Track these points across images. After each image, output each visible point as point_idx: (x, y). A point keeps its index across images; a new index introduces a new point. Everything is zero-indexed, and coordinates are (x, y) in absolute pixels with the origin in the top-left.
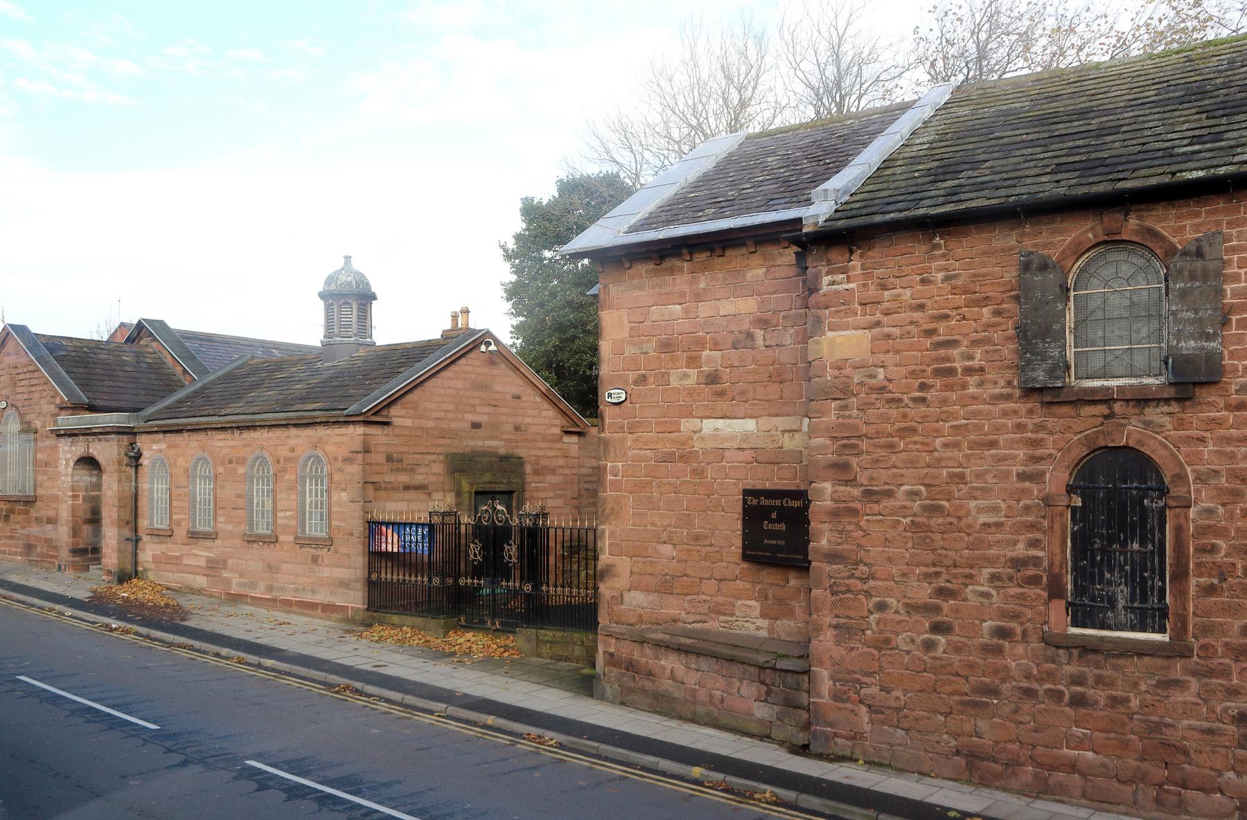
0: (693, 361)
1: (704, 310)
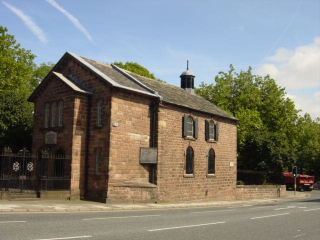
0: (130, 120)
1: (133, 108)
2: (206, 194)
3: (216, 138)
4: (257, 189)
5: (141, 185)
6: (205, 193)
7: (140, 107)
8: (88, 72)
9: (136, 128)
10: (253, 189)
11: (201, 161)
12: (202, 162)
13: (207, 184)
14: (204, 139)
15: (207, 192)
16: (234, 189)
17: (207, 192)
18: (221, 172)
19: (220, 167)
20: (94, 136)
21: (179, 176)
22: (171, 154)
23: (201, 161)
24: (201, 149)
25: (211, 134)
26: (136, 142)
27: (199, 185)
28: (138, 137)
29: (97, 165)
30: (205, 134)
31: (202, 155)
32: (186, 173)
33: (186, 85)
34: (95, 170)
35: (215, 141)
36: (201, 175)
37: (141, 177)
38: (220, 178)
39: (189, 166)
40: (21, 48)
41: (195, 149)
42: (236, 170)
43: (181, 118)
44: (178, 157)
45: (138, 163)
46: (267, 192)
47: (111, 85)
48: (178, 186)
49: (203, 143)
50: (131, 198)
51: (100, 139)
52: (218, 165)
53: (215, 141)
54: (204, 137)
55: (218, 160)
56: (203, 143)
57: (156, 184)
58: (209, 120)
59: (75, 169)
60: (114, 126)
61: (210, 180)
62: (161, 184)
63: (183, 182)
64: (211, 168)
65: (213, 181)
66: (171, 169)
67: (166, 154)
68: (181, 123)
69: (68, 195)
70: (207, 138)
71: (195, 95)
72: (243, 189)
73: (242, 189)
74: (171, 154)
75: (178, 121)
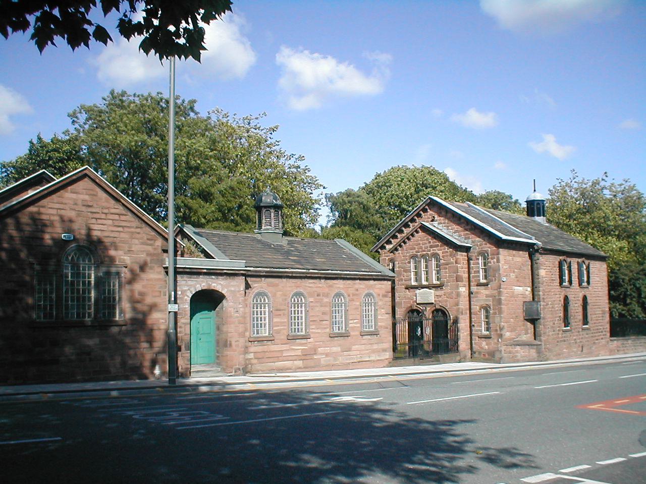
2: (582, 351)
3: (588, 282)
4: (630, 342)
5: (529, 343)
6: (580, 349)
7: (520, 256)
8: (462, 221)
9: (519, 282)
10: (625, 342)
11: (576, 308)
12: (577, 312)
13: (582, 338)
14: (578, 285)
15: (582, 347)
16: (608, 342)
17: (582, 347)
18: (595, 323)
19: (593, 316)
20: (477, 293)
21: (559, 330)
22: (551, 306)
23: (576, 308)
24: (576, 294)
25: (585, 281)
26: (483, 295)
27: (575, 340)
28: (519, 289)
29: (483, 324)
30: (578, 279)
31: (576, 304)
32: (565, 327)
33: (536, 213)
34: (394, 332)
35: (588, 286)
36: (576, 328)
37: (525, 334)
38: (594, 330)
39: (566, 321)
40: (302, 165)
41: (571, 297)
42: (608, 319)
43: (557, 263)
44: (557, 309)
45: (523, 319)
46: (641, 346)
47: (501, 238)
48: (558, 342)
49: (577, 289)
50: (521, 357)
51: (487, 296)
52: (591, 315)
53: (588, 286)
54: (578, 282)
55: (591, 308)
56: (577, 289)
57: (540, 341)
58: (580, 260)
59: (462, 329)
60: (503, 282)
61: (584, 332)
62: (545, 341)
63: (562, 338)
64: (585, 321)
65: (587, 334)
66: (551, 324)
67: (160, 286)
68: (558, 269)
69: (458, 358)
70: (580, 285)
71: (547, 225)
72: (616, 343)
73: (615, 342)
74: (551, 306)
75: (555, 267)
